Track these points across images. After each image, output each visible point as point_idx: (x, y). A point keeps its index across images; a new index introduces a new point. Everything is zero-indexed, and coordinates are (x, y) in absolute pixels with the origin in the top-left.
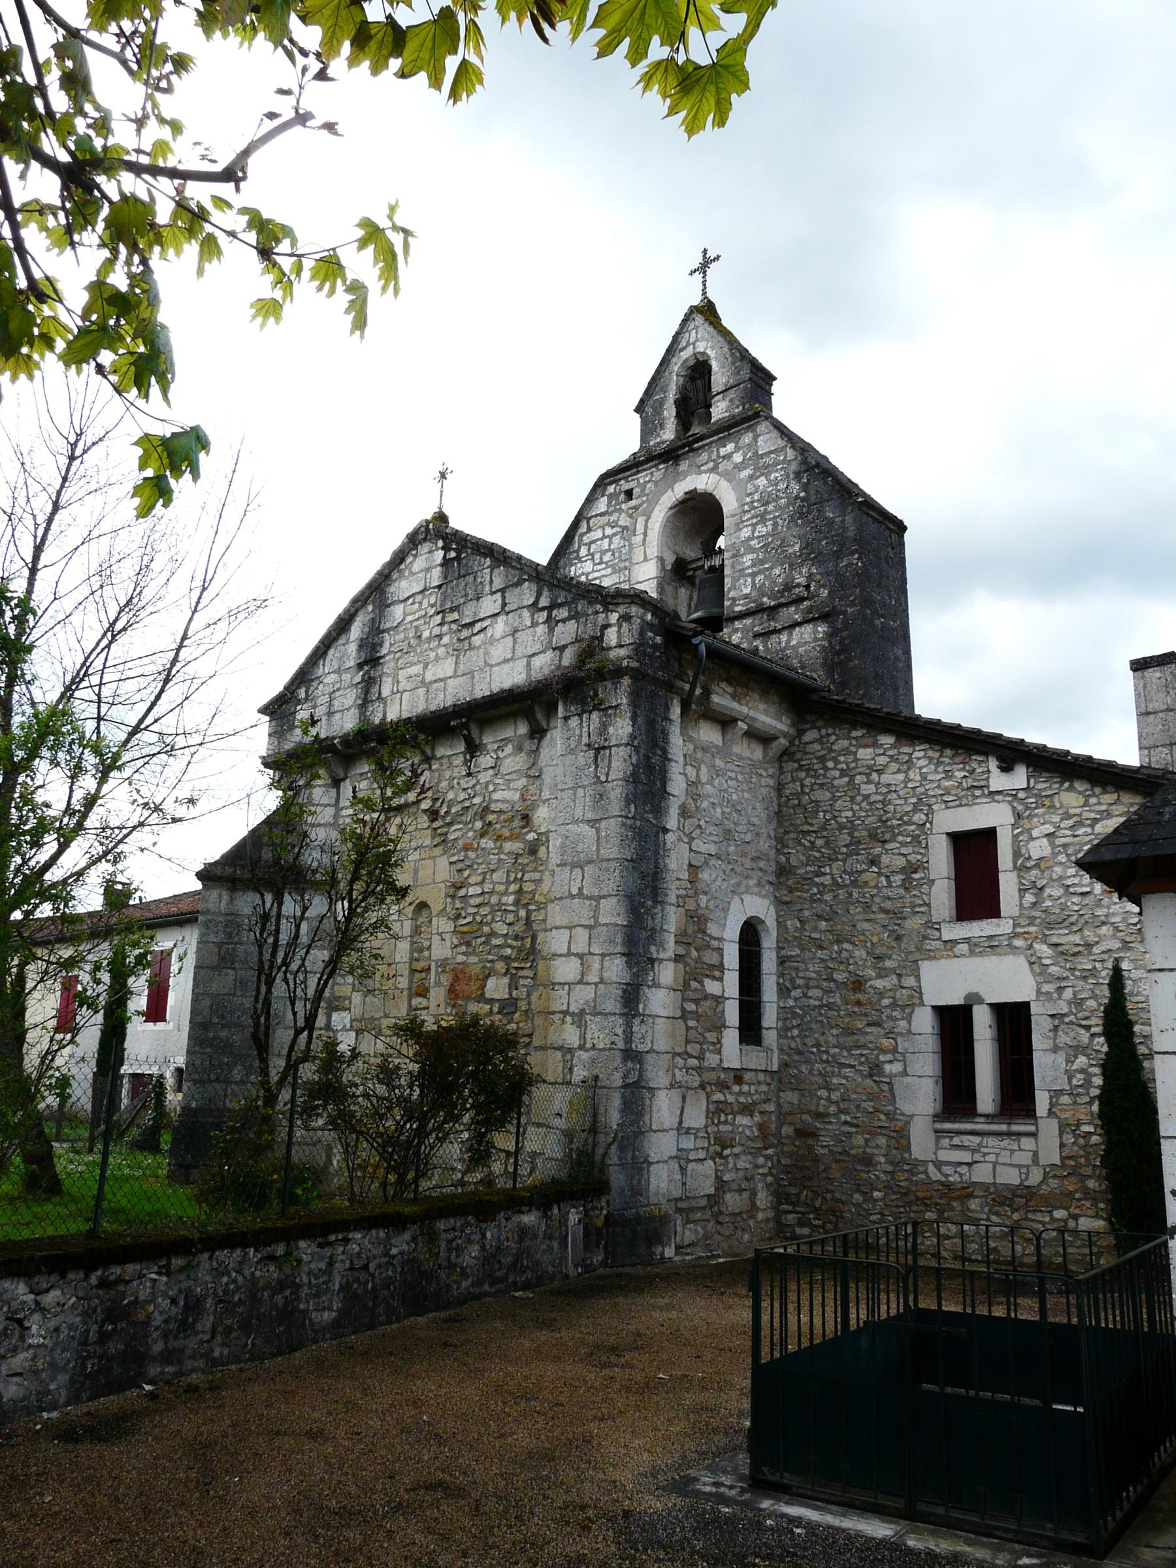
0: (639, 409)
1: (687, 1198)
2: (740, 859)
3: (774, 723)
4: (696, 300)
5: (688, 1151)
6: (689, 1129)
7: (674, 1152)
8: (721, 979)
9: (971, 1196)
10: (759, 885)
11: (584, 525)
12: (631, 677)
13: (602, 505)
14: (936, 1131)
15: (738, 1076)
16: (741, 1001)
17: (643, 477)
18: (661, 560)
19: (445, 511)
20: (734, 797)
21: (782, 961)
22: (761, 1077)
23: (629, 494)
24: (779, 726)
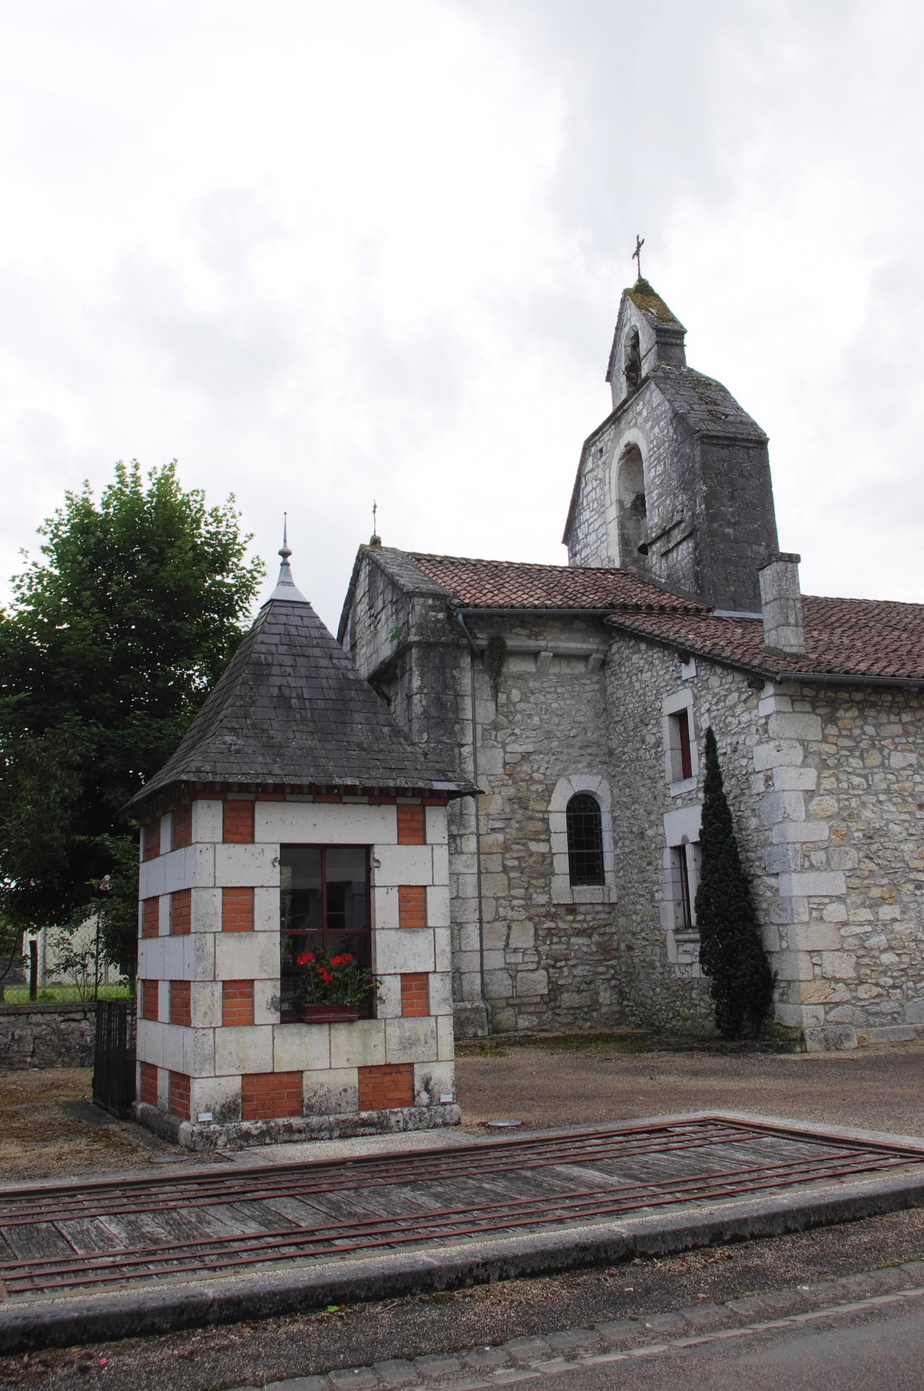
0: (608, 379)
1: (517, 996)
2: (566, 751)
3: (585, 646)
4: (631, 283)
5: (516, 964)
6: (516, 949)
7: (502, 965)
8: (548, 841)
9: (692, 989)
10: (590, 765)
11: (583, 480)
12: (417, 647)
13: (590, 465)
14: (677, 941)
15: (571, 909)
16: (570, 855)
17: (606, 437)
18: (620, 503)
19: (378, 535)
20: (554, 705)
21: (614, 819)
22: (600, 908)
23: (601, 451)
24: (590, 646)
